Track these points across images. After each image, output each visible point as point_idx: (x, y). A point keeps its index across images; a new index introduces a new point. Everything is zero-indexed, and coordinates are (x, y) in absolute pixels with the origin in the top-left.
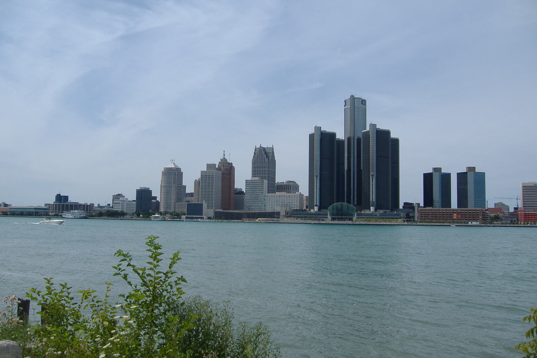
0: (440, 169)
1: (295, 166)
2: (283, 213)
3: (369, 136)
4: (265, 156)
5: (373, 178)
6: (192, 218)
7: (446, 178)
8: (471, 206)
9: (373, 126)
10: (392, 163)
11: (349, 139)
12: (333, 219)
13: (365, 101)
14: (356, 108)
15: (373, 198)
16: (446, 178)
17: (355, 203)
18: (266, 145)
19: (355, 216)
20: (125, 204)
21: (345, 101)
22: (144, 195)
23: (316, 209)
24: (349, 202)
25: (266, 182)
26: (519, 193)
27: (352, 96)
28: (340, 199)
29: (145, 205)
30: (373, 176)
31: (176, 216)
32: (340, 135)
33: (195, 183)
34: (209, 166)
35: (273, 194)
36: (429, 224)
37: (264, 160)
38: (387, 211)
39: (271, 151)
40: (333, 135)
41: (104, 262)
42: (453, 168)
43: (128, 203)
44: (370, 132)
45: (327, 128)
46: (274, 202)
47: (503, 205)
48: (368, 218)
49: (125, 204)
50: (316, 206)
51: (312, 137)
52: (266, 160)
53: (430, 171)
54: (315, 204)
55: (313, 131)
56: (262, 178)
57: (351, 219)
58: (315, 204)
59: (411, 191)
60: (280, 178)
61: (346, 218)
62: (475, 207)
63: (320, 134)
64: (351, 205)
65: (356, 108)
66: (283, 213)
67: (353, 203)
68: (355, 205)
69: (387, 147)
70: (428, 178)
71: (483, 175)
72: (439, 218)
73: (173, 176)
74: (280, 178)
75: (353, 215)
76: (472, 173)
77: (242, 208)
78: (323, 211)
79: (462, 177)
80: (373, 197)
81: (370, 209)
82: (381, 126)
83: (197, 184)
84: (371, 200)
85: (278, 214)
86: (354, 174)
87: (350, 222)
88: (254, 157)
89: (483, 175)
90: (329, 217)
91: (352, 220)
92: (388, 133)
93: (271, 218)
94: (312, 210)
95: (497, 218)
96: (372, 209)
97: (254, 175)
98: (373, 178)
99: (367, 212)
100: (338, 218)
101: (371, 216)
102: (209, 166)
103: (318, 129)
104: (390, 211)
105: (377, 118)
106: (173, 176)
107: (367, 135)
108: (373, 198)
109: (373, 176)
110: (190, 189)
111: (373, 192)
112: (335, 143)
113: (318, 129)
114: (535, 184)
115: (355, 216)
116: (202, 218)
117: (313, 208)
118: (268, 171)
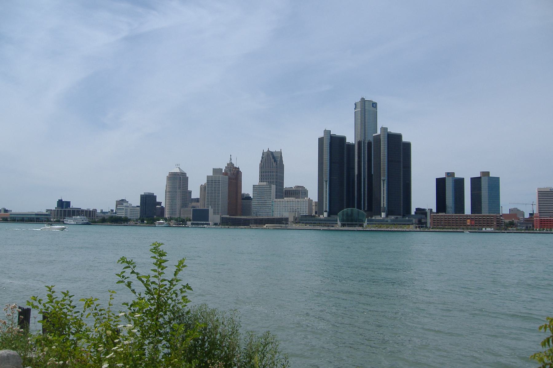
0: (453, 174)
1: (304, 171)
2: (291, 219)
3: (380, 139)
4: (273, 160)
5: (384, 183)
6: (198, 224)
7: (459, 183)
8: (485, 211)
9: (384, 129)
10: (404, 167)
11: (359, 143)
12: (343, 225)
13: (376, 104)
14: (367, 111)
15: (384, 204)
16: (459, 183)
17: (366, 209)
18: (274, 149)
19: (366, 222)
20: (129, 210)
21: (355, 104)
22: (148, 200)
23: (326, 215)
24: (359, 207)
25: (274, 187)
26: (535, 198)
27: (363, 99)
29: (149, 211)
30: (384, 181)
31: (181, 222)
32: (351, 139)
33: (201, 188)
34: (215, 171)
35: (281, 200)
36: (442, 230)
37: (272, 164)
38: (399, 217)
39: (279, 156)
40: (343, 139)
41: (107, 270)
42: (467, 173)
43: (132, 208)
44: (381, 136)
45: (337, 132)
46: (282, 208)
47: (518, 210)
48: (378, 224)
49: (129, 210)
50: (326, 211)
51: (321, 140)
52: (274, 164)
53: (443, 176)
54: (324, 210)
55: (322, 135)
56: (270, 183)
57: (361, 225)
58: (324, 210)
59: (423, 196)
60: (289, 183)
61: (356, 224)
62: (489, 213)
63: (329, 138)
64: (362, 211)
65: (367, 111)
66: (291, 219)
67: (364, 209)
68: (365, 211)
69: (399, 151)
70: (441, 183)
71: (497, 180)
72: (452, 224)
73: (178, 180)
74: (289, 183)
75: (363, 221)
76: (486, 178)
78: (333, 217)
79: (476, 182)
80: (384, 203)
81: (381, 215)
82: (393, 130)
83: (203, 189)
84: (382, 206)
85: (286, 220)
86: (365, 179)
87: (361, 228)
88: (261, 162)
89: (497, 180)
90: (339, 223)
91: (363, 226)
92: (399, 136)
93: (279, 224)
94: (321, 216)
95: (512, 224)
96: (383, 215)
97: (261, 180)
98: (384, 183)
99: (378, 218)
100: (348, 224)
101: (382, 222)
102: (215, 171)
103: (327, 132)
104: (401, 217)
105: (388, 122)
106: (178, 180)
107: (377, 139)
108: (384, 204)
109: (384, 181)
110: (196, 194)
111: (384, 197)
112: (345, 147)
113: (327, 132)
114: (551, 189)
115: (366, 222)
116: (208, 224)
117: (323, 214)
118: (276, 175)
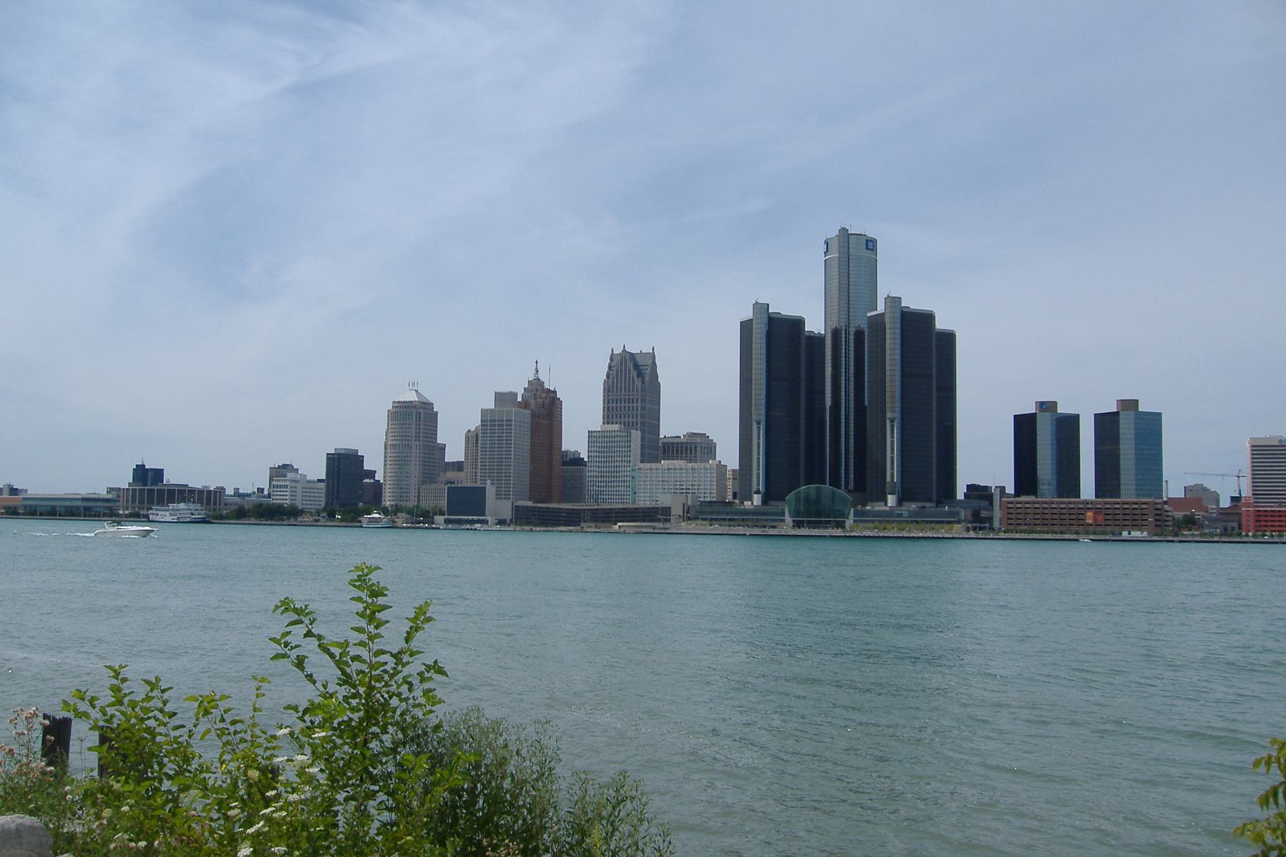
0: (1053, 405)
1: (706, 398)
2: (677, 510)
3: (883, 324)
4: (634, 373)
5: (892, 427)
6: (460, 522)
7: (1068, 425)
8: (1128, 492)
9: (893, 301)
10: (939, 389)
11: (836, 333)
12: (798, 524)
13: (874, 241)
14: (852, 259)
15: (892, 475)
16: (1068, 425)
17: (851, 487)
18: (636, 346)
19: (851, 516)
20: (299, 489)
21: (827, 243)
22: (344, 466)
23: (757, 500)
24: (835, 482)
25: (636, 435)
26: (1244, 462)
27: (844, 230)
28: (814, 476)
29: (347, 491)
30: (892, 421)
31: (422, 518)
32: (815, 324)
33: (467, 438)
34: (501, 398)
35: (654, 465)
36: (1027, 536)
37: (632, 383)
38: (927, 505)
39: (650, 363)
40: (797, 323)
41: (248, 628)
42: (1086, 402)
43: (308, 485)
44: (887, 316)
45: (784, 307)
46: (655, 484)
47: (1205, 490)
48: (880, 522)
49: (299, 489)
50: (758, 492)
51: (746, 327)
52: (638, 383)
53: (1031, 409)
54: (754, 488)
55: (748, 314)
56: (629, 426)
57: (840, 525)
58: (754, 488)
59: (984, 457)
60: (672, 426)
61: (829, 522)
62: (1138, 496)
63: (766, 320)
64: (842, 492)
65: (852, 259)
66: (677, 510)
67: (846, 487)
68: (849, 492)
69: (927, 351)
70: (1024, 427)
71: (1156, 418)
72: (1050, 522)
73: (414, 420)
74: (672, 426)
75: (845, 516)
76: (1131, 414)
77: (579, 498)
78: (775, 506)
79: (1107, 424)
80: (893, 472)
81: (886, 501)
82: (913, 302)
83: (472, 439)
84: (888, 479)
85: (666, 511)
86: (848, 418)
87: (839, 532)
88: (608, 376)
89: (1156, 418)
90: (789, 520)
91: (844, 527)
92: (928, 318)
93: (650, 521)
94: (748, 503)
95: (1190, 522)
96: (892, 500)
97: (608, 418)
98: (892, 427)
99: (879, 507)
100: (809, 522)
101: (887, 518)
102: (501, 398)
103: (761, 308)
104: (933, 505)
105: (902, 284)
106: (414, 420)
107: (878, 324)
108: (892, 475)
109: (892, 421)
110: (455, 452)
111: (892, 459)
112: (803, 342)
113: (761, 308)
114: (1280, 441)
115: (851, 516)
116: (485, 522)
117: (751, 499)
118: (643, 408)
